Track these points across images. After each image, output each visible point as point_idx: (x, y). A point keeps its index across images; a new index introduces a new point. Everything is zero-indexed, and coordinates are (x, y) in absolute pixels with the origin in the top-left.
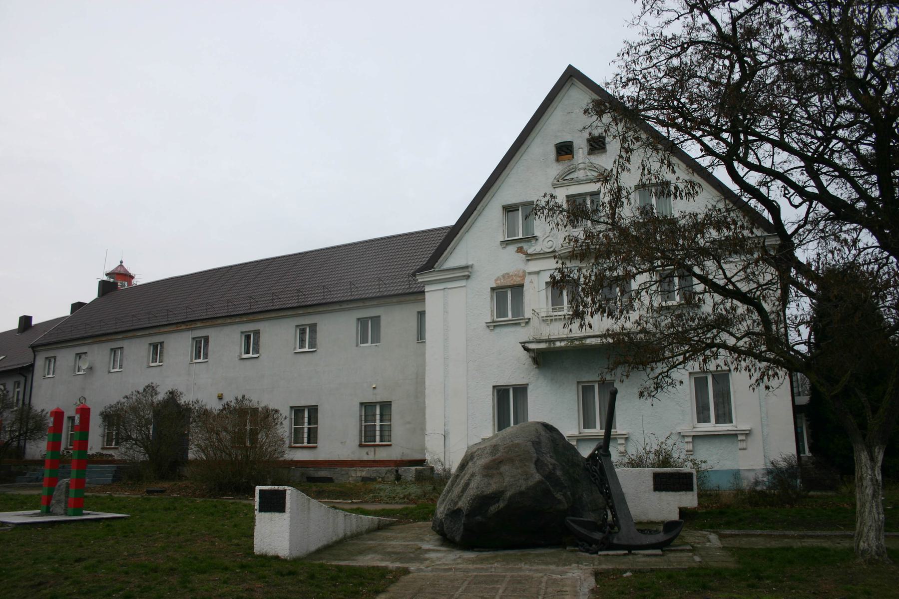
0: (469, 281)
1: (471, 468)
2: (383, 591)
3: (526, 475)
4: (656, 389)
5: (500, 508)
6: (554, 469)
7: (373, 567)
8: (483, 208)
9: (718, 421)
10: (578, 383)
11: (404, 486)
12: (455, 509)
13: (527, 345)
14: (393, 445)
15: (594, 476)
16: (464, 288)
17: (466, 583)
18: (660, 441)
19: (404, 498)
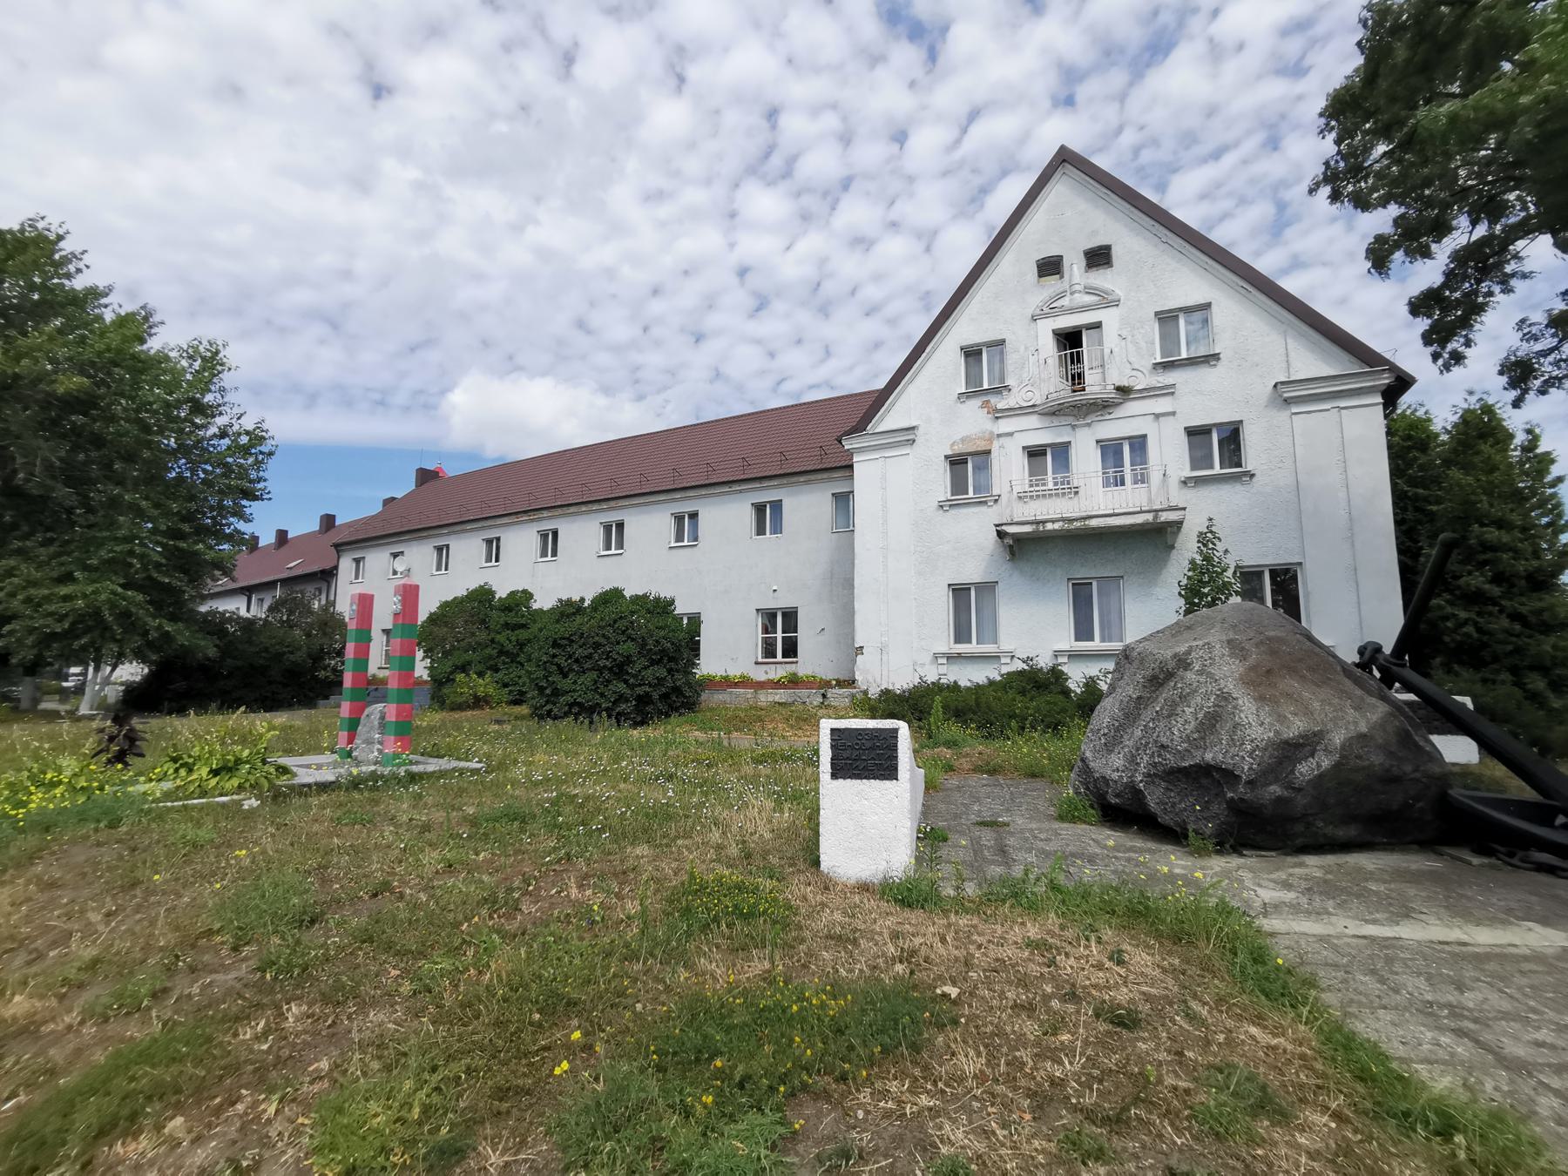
9: (1103, 640)
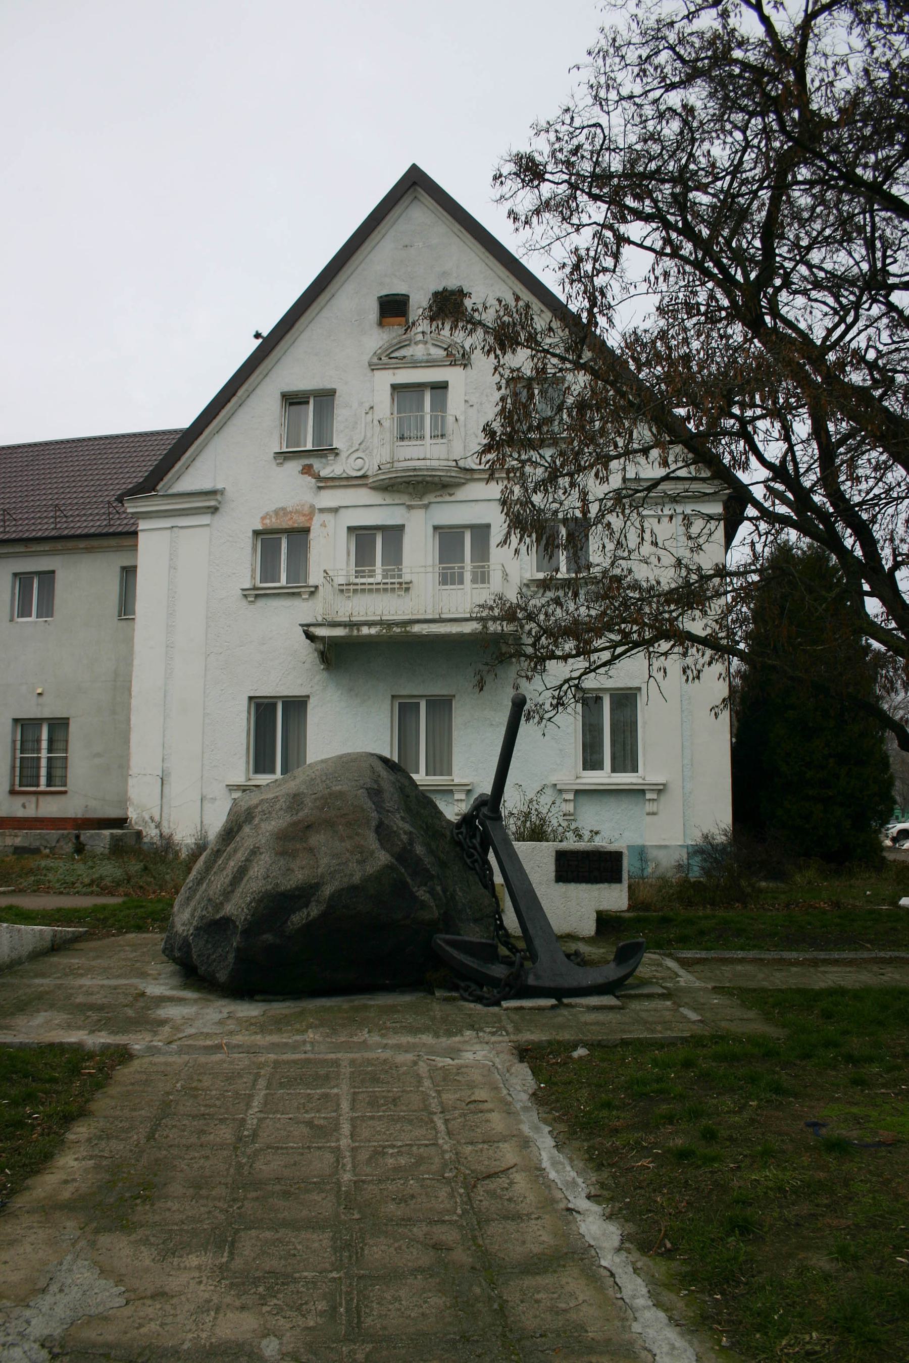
0: (217, 517)
1: (248, 838)
2: (83, 1113)
3: (361, 853)
4: (555, 707)
5: (310, 918)
6: (411, 842)
7: (51, 1045)
8: (247, 393)
10: (393, 697)
11: (90, 863)
12: (218, 917)
13: (312, 629)
14: (70, 793)
15: (471, 856)
16: (207, 528)
17: (262, 1083)
18: (527, 798)
19: (90, 885)
